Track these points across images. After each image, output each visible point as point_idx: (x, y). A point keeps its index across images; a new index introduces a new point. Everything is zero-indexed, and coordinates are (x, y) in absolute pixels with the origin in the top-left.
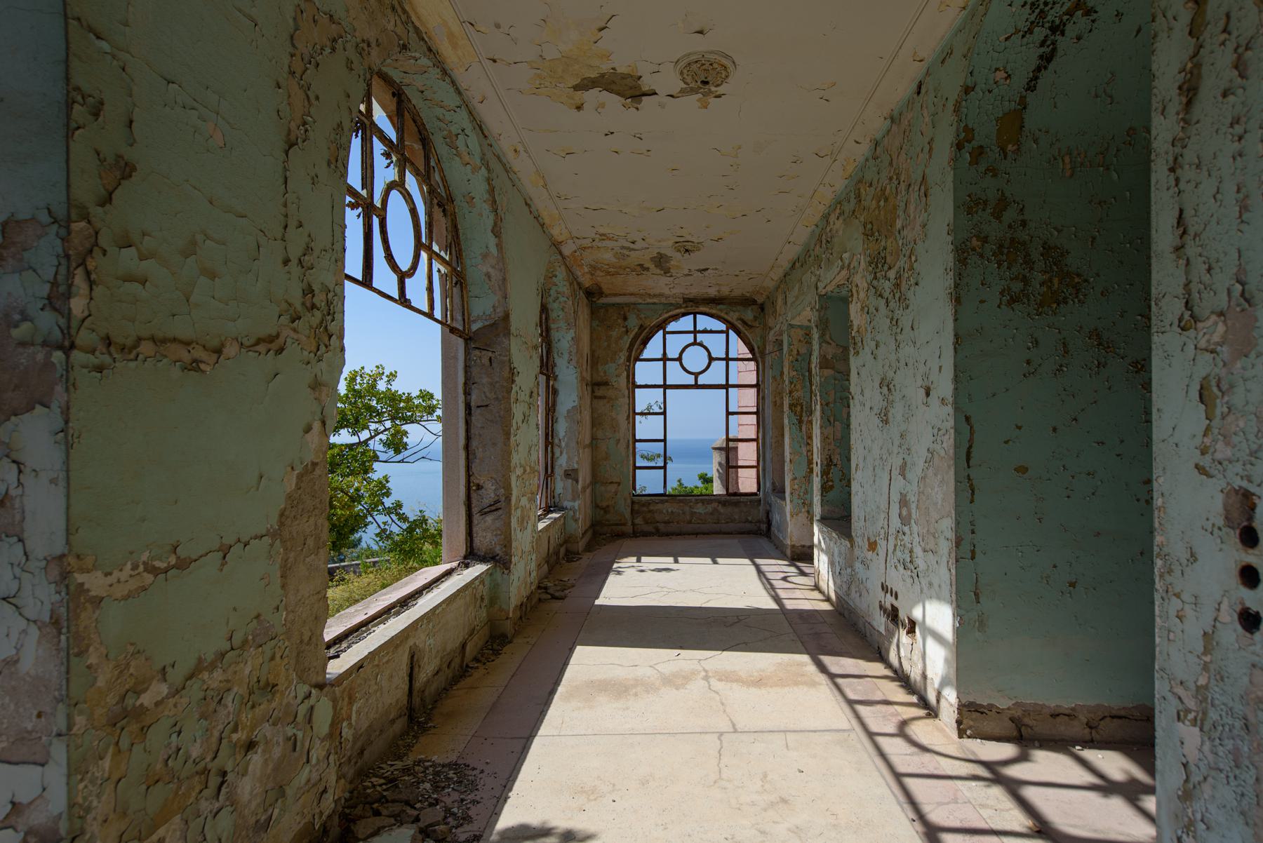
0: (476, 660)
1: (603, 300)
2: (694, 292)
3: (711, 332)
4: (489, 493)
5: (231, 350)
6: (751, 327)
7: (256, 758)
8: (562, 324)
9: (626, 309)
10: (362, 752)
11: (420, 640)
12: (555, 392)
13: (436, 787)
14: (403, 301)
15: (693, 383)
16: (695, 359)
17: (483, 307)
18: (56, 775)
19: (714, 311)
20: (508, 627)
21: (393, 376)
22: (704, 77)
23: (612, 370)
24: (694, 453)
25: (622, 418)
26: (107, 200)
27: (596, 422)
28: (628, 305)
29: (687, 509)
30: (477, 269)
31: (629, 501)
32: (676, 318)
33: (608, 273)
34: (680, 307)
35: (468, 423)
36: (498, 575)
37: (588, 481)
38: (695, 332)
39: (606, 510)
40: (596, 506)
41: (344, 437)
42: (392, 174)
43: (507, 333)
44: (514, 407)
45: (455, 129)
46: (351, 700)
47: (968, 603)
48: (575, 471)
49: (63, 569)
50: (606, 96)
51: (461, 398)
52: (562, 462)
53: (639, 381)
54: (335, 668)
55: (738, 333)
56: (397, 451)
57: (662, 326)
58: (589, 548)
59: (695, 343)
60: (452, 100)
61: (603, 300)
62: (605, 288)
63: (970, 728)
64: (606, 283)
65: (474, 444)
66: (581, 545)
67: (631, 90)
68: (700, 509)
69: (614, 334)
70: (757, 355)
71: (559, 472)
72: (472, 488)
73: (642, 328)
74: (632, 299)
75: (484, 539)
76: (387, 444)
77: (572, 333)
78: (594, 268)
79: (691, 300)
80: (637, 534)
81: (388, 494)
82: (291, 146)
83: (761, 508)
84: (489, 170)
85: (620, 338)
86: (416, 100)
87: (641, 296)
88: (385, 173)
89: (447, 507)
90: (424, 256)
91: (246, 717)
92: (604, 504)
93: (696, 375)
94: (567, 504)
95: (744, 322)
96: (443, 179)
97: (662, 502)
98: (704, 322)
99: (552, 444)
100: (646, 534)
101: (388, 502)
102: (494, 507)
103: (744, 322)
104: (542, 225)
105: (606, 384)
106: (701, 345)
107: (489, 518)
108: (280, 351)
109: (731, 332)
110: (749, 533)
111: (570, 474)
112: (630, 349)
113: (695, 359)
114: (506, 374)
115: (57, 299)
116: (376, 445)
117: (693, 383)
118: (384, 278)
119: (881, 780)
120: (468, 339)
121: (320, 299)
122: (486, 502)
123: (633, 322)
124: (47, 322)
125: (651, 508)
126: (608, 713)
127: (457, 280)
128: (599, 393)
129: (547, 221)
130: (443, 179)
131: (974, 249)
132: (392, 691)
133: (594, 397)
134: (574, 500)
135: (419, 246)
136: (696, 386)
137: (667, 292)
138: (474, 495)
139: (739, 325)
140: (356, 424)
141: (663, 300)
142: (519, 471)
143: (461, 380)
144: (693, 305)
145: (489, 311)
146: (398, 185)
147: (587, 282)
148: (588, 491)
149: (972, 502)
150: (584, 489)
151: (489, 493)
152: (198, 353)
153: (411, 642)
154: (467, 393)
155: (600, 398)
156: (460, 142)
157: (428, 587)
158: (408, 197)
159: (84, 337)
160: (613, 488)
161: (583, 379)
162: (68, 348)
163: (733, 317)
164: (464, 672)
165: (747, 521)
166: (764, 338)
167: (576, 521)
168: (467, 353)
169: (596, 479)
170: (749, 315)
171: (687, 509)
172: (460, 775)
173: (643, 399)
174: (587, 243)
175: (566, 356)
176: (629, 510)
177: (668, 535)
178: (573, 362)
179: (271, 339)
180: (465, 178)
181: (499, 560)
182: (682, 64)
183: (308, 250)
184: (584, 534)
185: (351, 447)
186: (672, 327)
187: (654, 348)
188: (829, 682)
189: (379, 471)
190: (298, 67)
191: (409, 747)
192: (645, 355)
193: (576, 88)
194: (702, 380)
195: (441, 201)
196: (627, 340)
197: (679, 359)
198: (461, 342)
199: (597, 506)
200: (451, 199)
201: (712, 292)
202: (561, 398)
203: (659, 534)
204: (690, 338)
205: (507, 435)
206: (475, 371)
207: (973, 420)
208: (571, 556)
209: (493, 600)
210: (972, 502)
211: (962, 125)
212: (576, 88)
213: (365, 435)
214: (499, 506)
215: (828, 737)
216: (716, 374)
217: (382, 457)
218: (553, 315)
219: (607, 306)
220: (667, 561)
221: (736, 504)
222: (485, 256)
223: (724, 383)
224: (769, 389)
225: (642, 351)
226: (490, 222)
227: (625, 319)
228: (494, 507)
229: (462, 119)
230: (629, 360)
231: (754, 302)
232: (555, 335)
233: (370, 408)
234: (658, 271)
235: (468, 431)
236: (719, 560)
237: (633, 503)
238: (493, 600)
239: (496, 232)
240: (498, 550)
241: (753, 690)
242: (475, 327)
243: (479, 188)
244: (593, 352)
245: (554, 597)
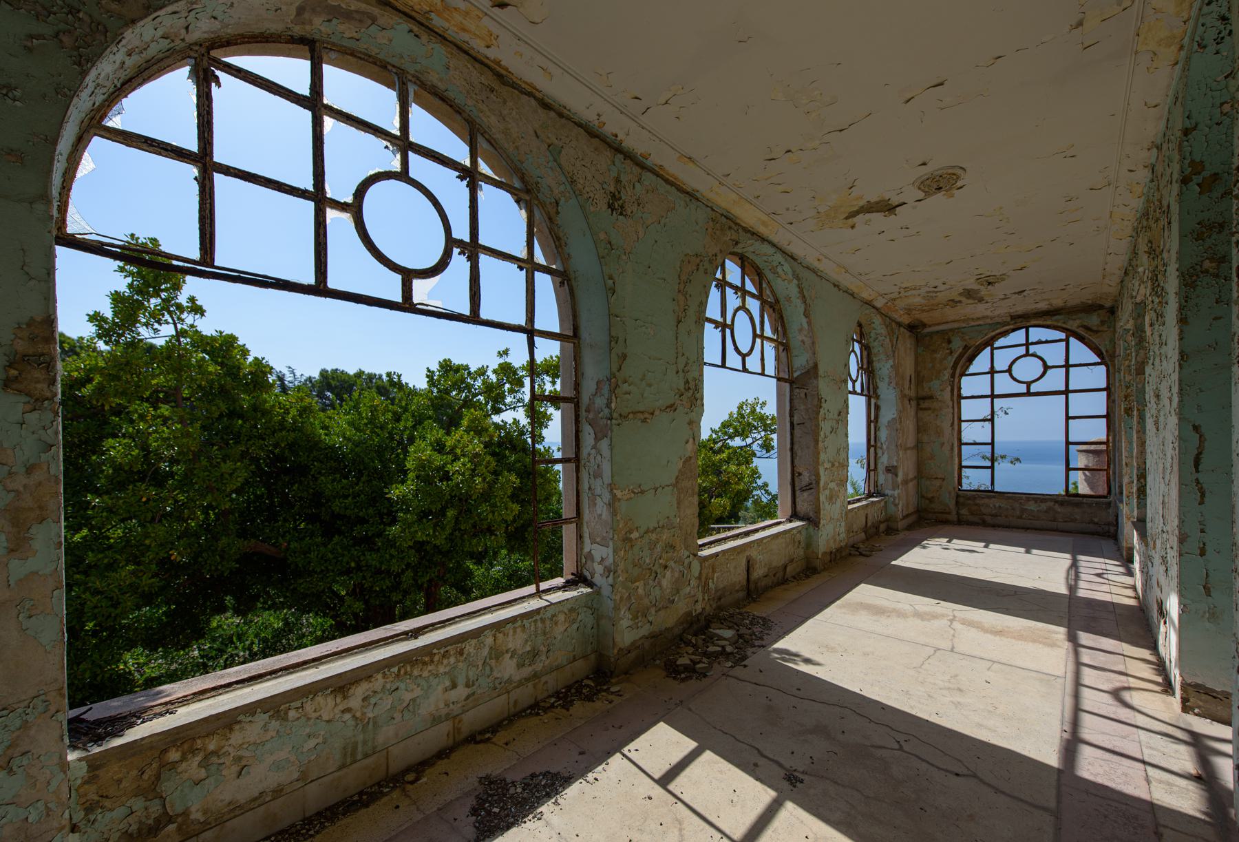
0: (794, 577)
1: (927, 330)
2: (1020, 309)
3: (1047, 342)
4: (806, 478)
5: (657, 413)
6: (1097, 332)
7: (668, 574)
8: (883, 357)
10: (720, 599)
11: (754, 553)
12: (877, 408)
13: (751, 623)
14: (745, 370)
15: (1025, 391)
16: (1028, 369)
17: (801, 361)
18: (610, 550)
19: (1049, 323)
20: (818, 564)
21: (764, 403)
22: (940, 183)
23: (938, 386)
24: (1037, 454)
25: (946, 425)
26: (620, 369)
27: (920, 429)
28: (951, 330)
29: (1017, 505)
30: (796, 338)
31: (953, 494)
32: (1005, 334)
33: (923, 311)
34: (1008, 324)
35: (792, 434)
36: (811, 529)
37: (911, 476)
38: (1027, 344)
39: (931, 500)
40: (922, 497)
41: (737, 442)
42: (738, 303)
43: (817, 377)
44: (822, 424)
45: (775, 264)
46: (714, 571)
47: (1181, 596)
48: (895, 467)
49: (611, 487)
50: (868, 216)
51: (788, 419)
52: (884, 460)
54: (705, 552)
55: (1081, 339)
56: (768, 451)
57: (989, 343)
58: (909, 528)
60: (771, 250)
61: (927, 330)
62: (925, 321)
63: (1199, 707)
64: (925, 317)
65: (796, 447)
66: (901, 525)
67: (888, 208)
68: (1032, 506)
70: (1106, 357)
71: (881, 468)
72: (795, 475)
73: (966, 348)
74: (955, 325)
75: (803, 507)
76: (762, 446)
77: (891, 362)
78: (908, 311)
79: (1020, 317)
80: (960, 522)
81: (759, 477)
82: (679, 322)
83: (1110, 511)
84: (798, 278)
86: (751, 256)
87: (964, 321)
88: (733, 301)
89: (780, 485)
90: (758, 341)
91: (664, 556)
92: (930, 495)
93: (1029, 384)
94: (887, 492)
96: (773, 292)
97: (989, 497)
98: (1036, 333)
99: (875, 446)
100: (970, 524)
101: (760, 482)
102: (808, 487)
103: (1087, 328)
104: (852, 295)
105: (931, 398)
106: (1034, 355)
107: (805, 494)
109: (1072, 339)
110: (1092, 534)
111: (891, 470)
112: (954, 367)
114: (816, 402)
115: (608, 405)
116: (755, 447)
117: (1025, 391)
118: (734, 360)
119: (1059, 708)
120: (791, 382)
121: (692, 385)
122: (804, 483)
123: (957, 344)
124: (606, 411)
126: (864, 620)
127: (784, 347)
128: (923, 405)
129: (855, 290)
130: (773, 292)
131: (1207, 271)
132: (735, 575)
133: (919, 408)
134: (894, 489)
135: (755, 336)
137: (988, 313)
138: (796, 480)
139: (1082, 332)
140: (743, 434)
141: (989, 321)
142: (827, 465)
143: (788, 408)
144: (1022, 321)
145: (804, 363)
146: (743, 307)
147: (906, 320)
148: (911, 485)
149: (1201, 503)
150: (905, 482)
151: (806, 478)
152: (647, 415)
153: (747, 553)
154: (791, 416)
155: (926, 409)
156: (779, 270)
157: (763, 528)
158: (748, 312)
159: (615, 415)
160: (938, 483)
161: (903, 396)
162: (611, 419)
163: (1073, 325)
164: (784, 581)
166: (1113, 342)
167: (896, 505)
168: (791, 391)
169: (921, 473)
170: (1094, 320)
171: (1017, 505)
172: (766, 622)
173: (970, 409)
174: (895, 295)
175: (887, 380)
176: (954, 502)
177: (994, 526)
178: (893, 384)
179: (671, 406)
180: (786, 287)
181: (813, 520)
182: (917, 184)
183: (687, 364)
184: (904, 517)
185: (741, 448)
186: (1001, 342)
187: (981, 362)
188: (1071, 649)
189: (756, 462)
190: (682, 287)
191: (745, 606)
192: (972, 370)
193: (846, 218)
194: (1034, 388)
195: (772, 306)
196: (951, 360)
198: (787, 385)
199: (923, 497)
200: (777, 301)
201: (1043, 306)
202: (882, 412)
203: (984, 524)
204: (1022, 350)
205: (817, 442)
206: (796, 402)
207: (1203, 430)
208: (890, 531)
209: (808, 545)
210: (1201, 503)
211: (1187, 162)
212: (846, 218)
213: (749, 441)
214: (813, 486)
215: (1034, 674)
216: (1055, 380)
217: (758, 454)
218: (874, 351)
219: (931, 334)
220: (978, 546)
221: (1078, 505)
222: (800, 330)
223: (1063, 389)
224: (1119, 393)
225: (968, 367)
226: (802, 310)
227: (949, 342)
228: (808, 487)
229: (779, 257)
230: (953, 375)
231: (1101, 307)
232: (876, 365)
233: (749, 424)
234: (971, 301)
235: (792, 439)
236: (1034, 551)
237: (958, 496)
238: (808, 545)
239: (806, 314)
240: (811, 514)
241: (998, 638)
242: (795, 375)
243: (793, 290)
244: (917, 373)
245: (861, 554)
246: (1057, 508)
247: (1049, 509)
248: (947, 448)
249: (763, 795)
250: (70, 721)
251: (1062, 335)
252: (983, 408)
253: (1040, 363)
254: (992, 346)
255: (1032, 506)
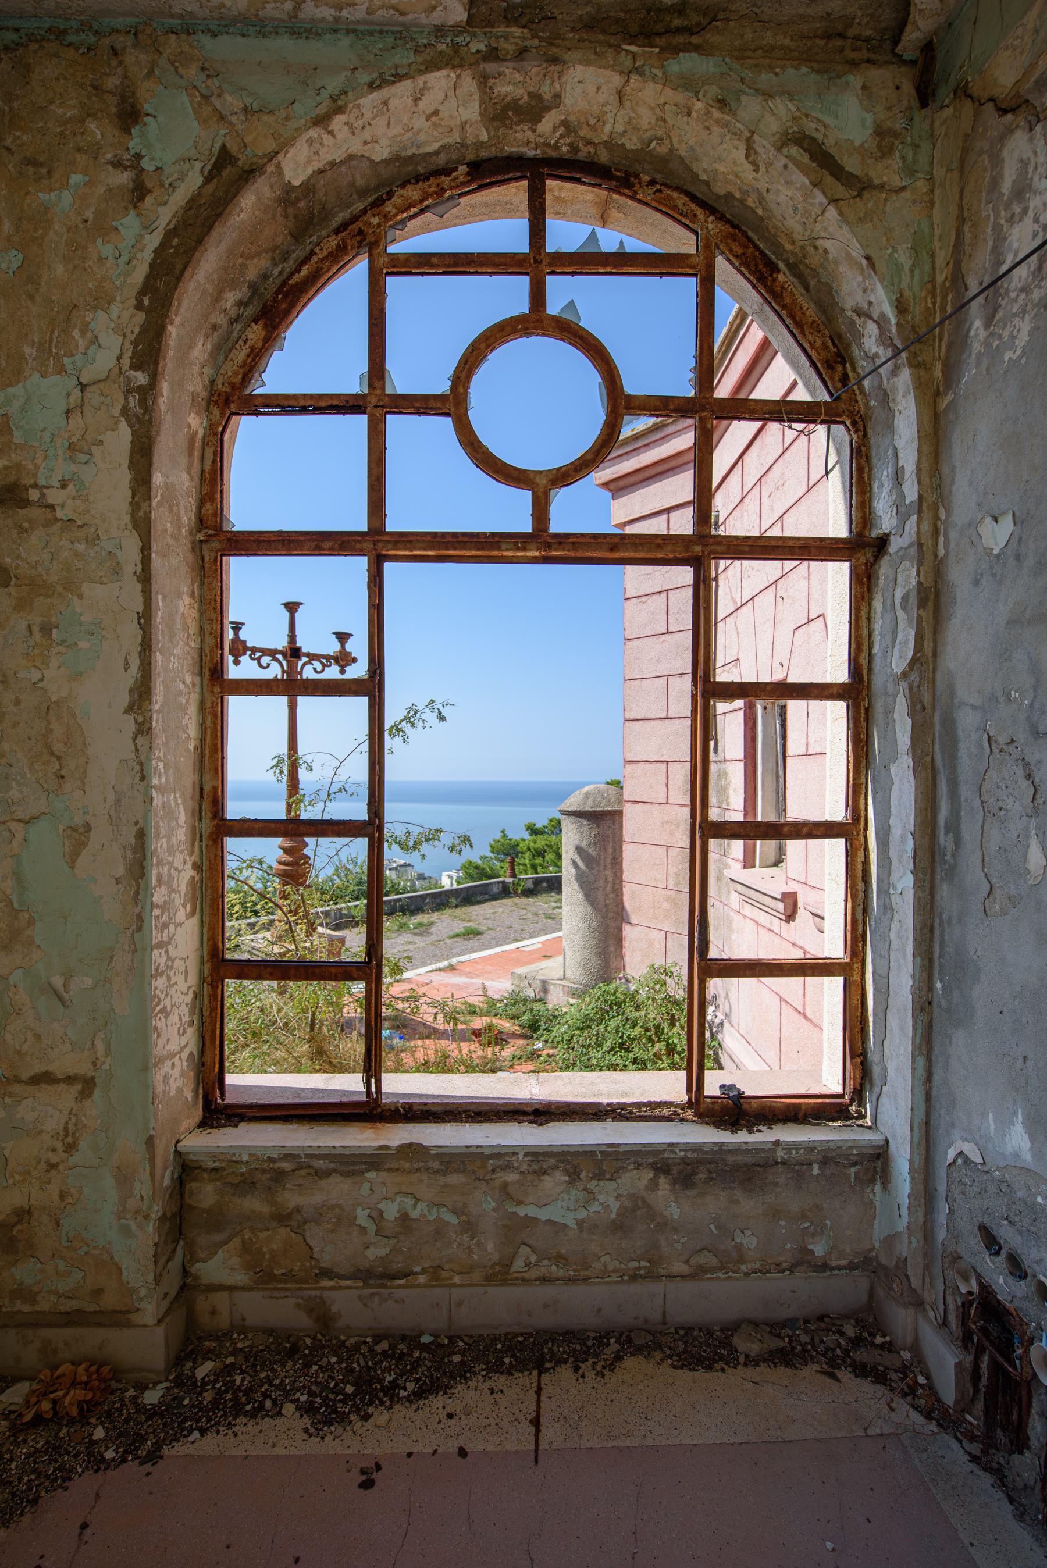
9: (135, 59)
16: (538, 406)
29: (485, 1204)
53: (243, 514)
59: (535, 321)
69: (63, 200)
85: (102, 228)
95: (823, 162)
106: (569, 331)
108: (452, 849)
113: (538, 406)
125: (291, 1198)
136: (545, 545)
160: (48, 1111)
165: (804, 1260)
171: (485, 1204)
187: (319, 346)
192: (277, 376)
194: (574, 511)
196: (135, 243)
197: (451, 404)
204: (510, 296)
227: (130, 116)
246: (669, 1203)
247: (637, 1207)
248: (105, 858)
249: (672, 533)
250: (560, 930)
251: (681, 241)
252: (329, 598)
253: (592, 378)
254: (370, 243)
255: (273, 825)
